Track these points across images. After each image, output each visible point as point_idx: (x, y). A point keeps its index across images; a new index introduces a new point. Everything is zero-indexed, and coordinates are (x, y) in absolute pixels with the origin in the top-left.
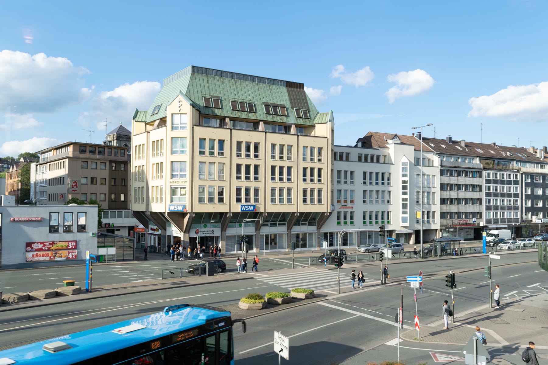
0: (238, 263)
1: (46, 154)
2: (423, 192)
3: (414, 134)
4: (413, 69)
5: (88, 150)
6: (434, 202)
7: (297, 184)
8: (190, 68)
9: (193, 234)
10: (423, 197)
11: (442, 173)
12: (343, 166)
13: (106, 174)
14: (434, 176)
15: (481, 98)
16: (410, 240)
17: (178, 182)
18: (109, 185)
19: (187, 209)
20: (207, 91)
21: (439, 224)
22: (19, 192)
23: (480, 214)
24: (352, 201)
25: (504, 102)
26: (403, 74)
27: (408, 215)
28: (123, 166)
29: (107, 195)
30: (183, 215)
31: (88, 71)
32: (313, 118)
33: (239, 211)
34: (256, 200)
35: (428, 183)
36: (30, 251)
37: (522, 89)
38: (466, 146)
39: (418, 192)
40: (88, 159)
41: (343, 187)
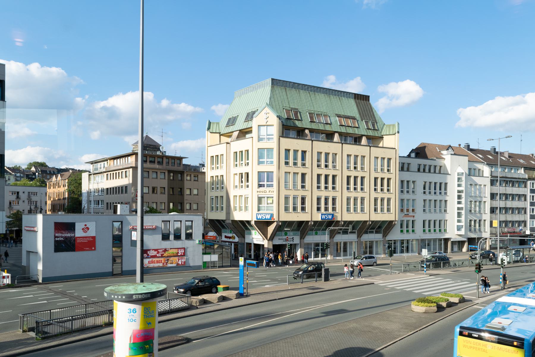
0: (346, 269)
1: (99, 164)
2: (475, 202)
3: (460, 145)
4: (402, 80)
5: (156, 162)
6: (485, 211)
7: (369, 193)
8: (269, 81)
9: (277, 242)
10: (475, 206)
11: (492, 183)
12: (407, 176)
13: (165, 183)
14: (485, 185)
15: (469, 109)
16: (463, 247)
17: (266, 191)
18: (168, 194)
19: (275, 217)
20: (287, 103)
21: (489, 233)
22: (66, 201)
23: (525, 222)
24: (413, 210)
25: (491, 112)
26: (393, 84)
27: (463, 224)
28: (179, 175)
29: (166, 204)
30: (268, 223)
31: (82, 81)
32: (380, 129)
33: (320, 219)
34: (334, 209)
35: (480, 193)
36: (147, 258)
37: (510, 99)
38: (509, 157)
39: (471, 201)
40: (149, 169)
41: (406, 196)
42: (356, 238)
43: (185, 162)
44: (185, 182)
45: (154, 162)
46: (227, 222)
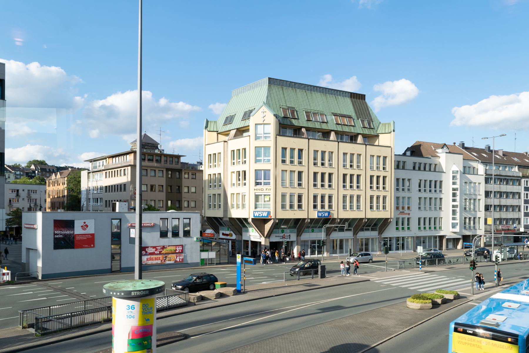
0: (342, 266)
1: (98, 162)
2: (470, 199)
3: (455, 143)
4: (398, 79)
5: (154, 160)
6: (479, 208)
7: (365, 191)
8: (266, 80)
9: (274, 239)
10: (470, 203)
11: (487, 181)
12: (402, 174)
13: (163, 181)
14: (479, 183)
15: (463, 107)
16: (457, 244)
17: (263, 189)
18: (166, 192)
19: (272, 215)
20: (284, 102)
21: (484, 230)
22: (66, 198)
23: (519, 220)
24: (409, 208)
25: (486, 111)
26: (388, 83)
27: (458, 221)
28: (177, 173)
29: (165, 201)
30: (265, 221)
31: (81, 80)
32: (376, 128)
33: (316, 217)
34: (330, 207)
35: (475, 191)
36: (145, 255)
37: (504, 98)
38: (504, 155)
39: (466, 199)
40: (148, 167)
41: (401, 194)
42: (352, 235)
43: (182, 160)
44: (183, 180)
45: (152, 160)
46: (225, 219)
